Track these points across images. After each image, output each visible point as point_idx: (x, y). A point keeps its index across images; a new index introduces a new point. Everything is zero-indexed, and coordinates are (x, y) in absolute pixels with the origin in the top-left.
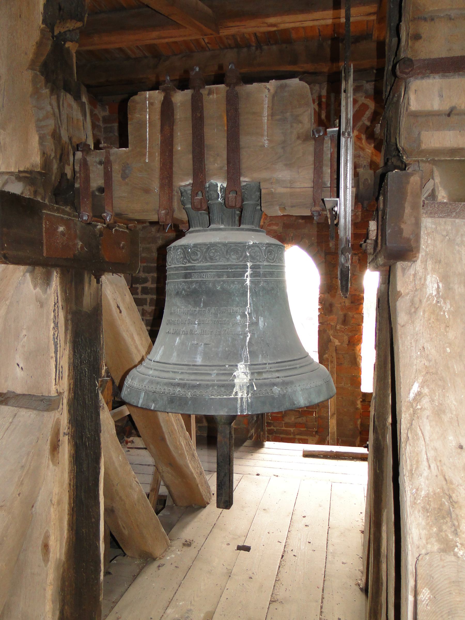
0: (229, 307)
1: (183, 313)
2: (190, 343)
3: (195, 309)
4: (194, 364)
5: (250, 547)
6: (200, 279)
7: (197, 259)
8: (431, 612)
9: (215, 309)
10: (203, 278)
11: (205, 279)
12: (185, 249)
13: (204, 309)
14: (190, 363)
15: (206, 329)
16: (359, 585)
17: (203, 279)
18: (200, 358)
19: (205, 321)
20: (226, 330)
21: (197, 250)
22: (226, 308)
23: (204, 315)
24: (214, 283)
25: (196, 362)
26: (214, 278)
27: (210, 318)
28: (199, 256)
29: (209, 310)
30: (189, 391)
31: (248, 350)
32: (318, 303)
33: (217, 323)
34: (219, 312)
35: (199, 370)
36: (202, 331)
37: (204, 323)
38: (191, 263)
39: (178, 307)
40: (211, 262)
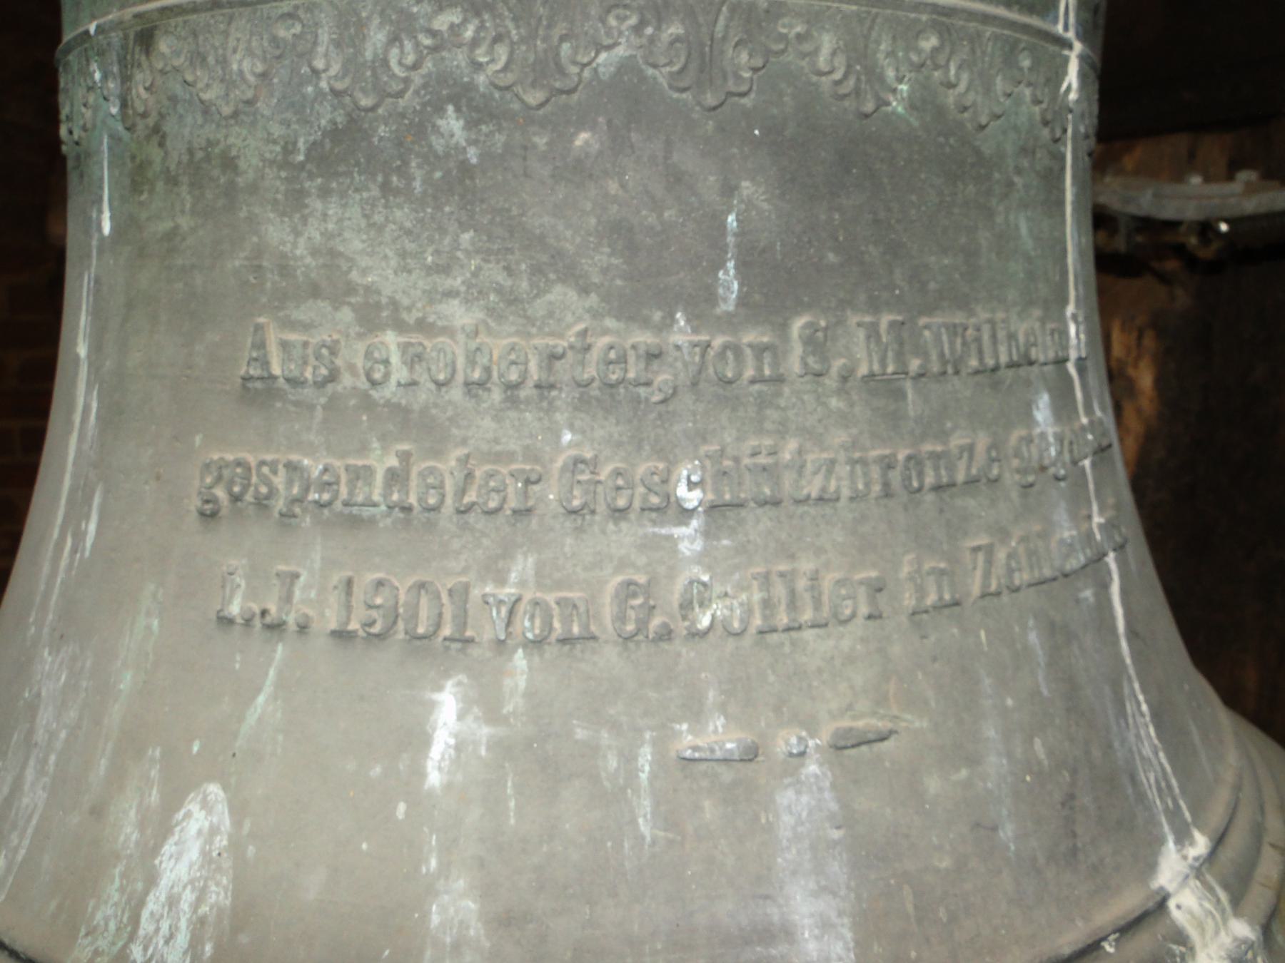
0: (983, 315)
2: (645, 756)
3: (644, 338)
8: (171, 856)
13: (750, 337)
19: (788, 480)
22: (959, 318)
23: (763, 403)
27: (840, 437)
29: (815, 343)
34: (915, 364)
36: (780, 591)
37: (776, 503)
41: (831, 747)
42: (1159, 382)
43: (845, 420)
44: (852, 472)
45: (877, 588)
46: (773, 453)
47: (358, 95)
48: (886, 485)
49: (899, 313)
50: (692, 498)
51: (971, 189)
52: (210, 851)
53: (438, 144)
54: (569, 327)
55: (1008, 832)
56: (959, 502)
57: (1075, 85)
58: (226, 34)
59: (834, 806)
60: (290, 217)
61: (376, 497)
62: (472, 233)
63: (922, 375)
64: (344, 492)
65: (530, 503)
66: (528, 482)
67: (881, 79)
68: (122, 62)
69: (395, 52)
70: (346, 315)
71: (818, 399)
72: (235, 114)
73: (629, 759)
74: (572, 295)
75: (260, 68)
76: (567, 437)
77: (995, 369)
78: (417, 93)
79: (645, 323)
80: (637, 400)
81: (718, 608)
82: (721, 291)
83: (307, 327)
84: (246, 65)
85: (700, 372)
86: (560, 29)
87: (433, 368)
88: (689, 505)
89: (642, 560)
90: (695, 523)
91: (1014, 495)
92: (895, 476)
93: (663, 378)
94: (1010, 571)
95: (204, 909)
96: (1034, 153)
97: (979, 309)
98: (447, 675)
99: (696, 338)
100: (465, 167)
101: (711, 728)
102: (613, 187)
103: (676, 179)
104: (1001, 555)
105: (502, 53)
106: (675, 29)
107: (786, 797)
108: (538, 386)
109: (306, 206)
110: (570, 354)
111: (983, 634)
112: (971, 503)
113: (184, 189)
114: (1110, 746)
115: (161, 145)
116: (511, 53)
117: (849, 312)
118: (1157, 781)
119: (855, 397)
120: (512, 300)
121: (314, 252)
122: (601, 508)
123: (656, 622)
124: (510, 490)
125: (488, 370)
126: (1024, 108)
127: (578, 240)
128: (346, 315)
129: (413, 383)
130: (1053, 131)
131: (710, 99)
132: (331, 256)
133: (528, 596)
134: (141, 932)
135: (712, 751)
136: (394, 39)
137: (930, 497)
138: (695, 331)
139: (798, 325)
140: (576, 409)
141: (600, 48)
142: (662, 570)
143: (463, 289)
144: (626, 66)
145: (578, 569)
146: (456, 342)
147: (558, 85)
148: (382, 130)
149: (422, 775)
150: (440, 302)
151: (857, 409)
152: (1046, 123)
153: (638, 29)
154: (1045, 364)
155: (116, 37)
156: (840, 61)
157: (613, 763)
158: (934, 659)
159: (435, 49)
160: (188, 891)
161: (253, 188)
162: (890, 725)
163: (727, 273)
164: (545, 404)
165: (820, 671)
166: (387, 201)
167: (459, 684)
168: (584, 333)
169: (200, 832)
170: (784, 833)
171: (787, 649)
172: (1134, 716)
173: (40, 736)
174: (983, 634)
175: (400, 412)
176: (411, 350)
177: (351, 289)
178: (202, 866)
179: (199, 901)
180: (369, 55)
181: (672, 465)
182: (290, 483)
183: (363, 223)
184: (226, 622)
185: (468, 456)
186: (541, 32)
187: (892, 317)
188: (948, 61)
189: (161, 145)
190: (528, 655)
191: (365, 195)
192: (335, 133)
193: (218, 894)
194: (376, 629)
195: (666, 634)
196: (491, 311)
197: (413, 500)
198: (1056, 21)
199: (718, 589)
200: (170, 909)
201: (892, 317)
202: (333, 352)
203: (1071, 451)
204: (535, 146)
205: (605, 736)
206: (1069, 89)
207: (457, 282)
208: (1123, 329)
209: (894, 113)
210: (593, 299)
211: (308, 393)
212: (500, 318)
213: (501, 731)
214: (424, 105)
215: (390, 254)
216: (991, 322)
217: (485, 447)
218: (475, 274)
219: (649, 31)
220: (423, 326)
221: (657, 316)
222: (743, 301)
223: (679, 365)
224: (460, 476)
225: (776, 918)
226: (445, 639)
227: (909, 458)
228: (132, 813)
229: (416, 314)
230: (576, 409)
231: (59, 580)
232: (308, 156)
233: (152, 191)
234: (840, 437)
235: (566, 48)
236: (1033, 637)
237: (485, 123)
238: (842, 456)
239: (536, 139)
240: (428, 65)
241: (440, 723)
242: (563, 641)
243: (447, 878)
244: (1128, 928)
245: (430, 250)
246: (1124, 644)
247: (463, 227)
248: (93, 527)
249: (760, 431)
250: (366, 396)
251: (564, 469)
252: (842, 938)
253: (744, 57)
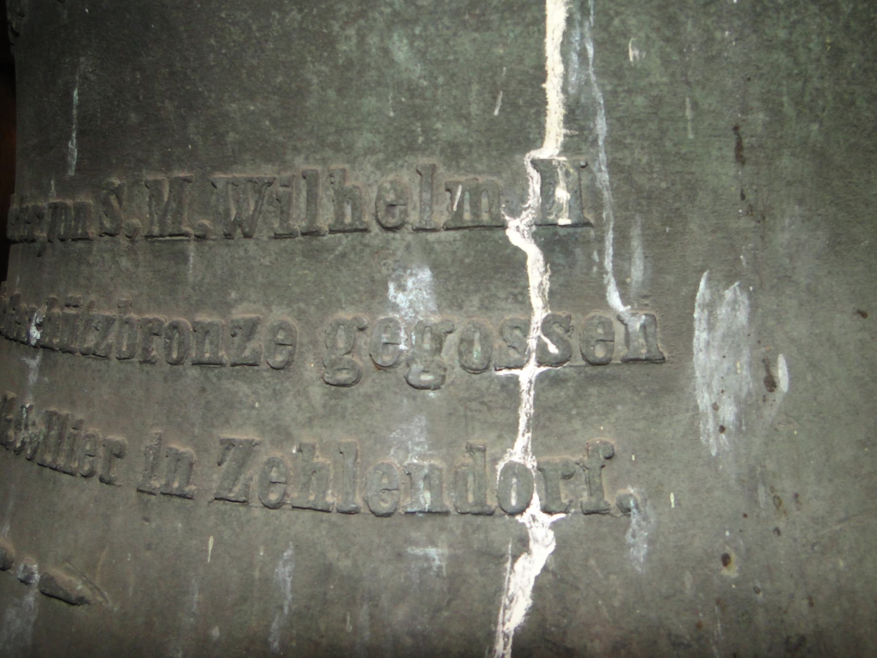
0: (300, 163)
20: (250, 448)
22: (267, 171)
41: (854, 314)
56: (227, 384)
77: (312, 233)
111: (211, 541)
112: (243, 389)
117: (144, 172)
151: (141, 269)
162: (87, 593)
163: (72, 144)
174: (211, 541)
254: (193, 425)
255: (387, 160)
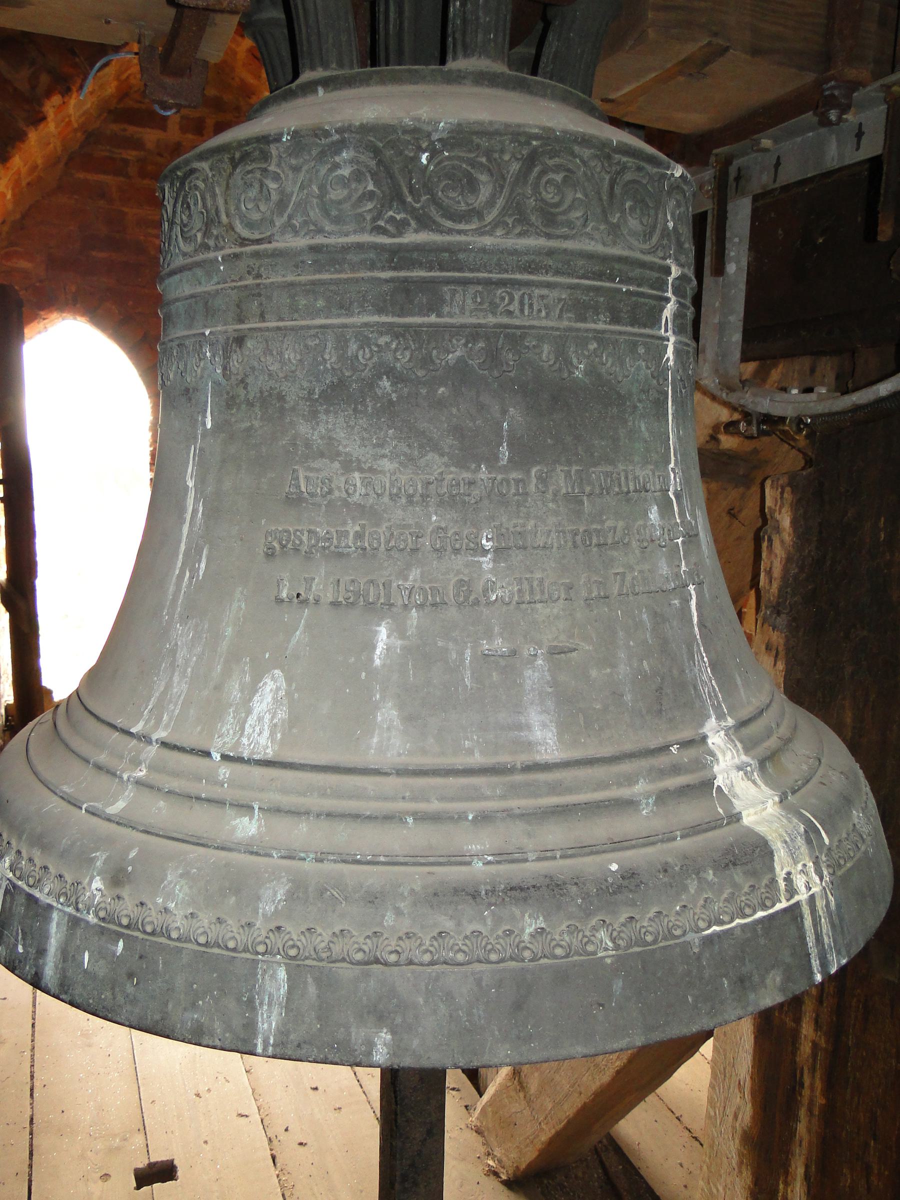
0: (621, 467)
1: (394, 497)
2: (468, 653)
3: (467, 475)
4: (523, 758)
5: (172, 1161)
6: (491, 320)
7: (478, 214)
9: (568, 474)
10: (510, 313)
11: (517, 322)
12: (389, 153)
13: (514, 475)
14: (504, 758)
15: (538, 575)
16: (496, 1174)
17: (505, 320)
18: (544, 726)
20: (623, 575)
21: (473, 163)
22: (609, 468)
23: (519, 505)
24: (561, 342)
25: (529, 746)
26: (560, 317)
27: (552, 520)
28: (485, 192)
29: (543, 480)
30: (593, 922)
31: (706, 659)
32: (148, 467)
33: (583, 541)
34: (588, 489)
35: (570, 790)
36: (526, 586)
37: (525, 548)
38: (440, 230)
39: (348, 465)
40: (549, 236)
42: (794, 522)
43: (556, 513)
44: (558, 536)
45: (569, 588)
46: (524, 526)
47: (345, 371)
48: (574, 542)
49: (580, 466)
50: (488, 545)
51: (615, 410)
52: (277, 697)
53: (379, 392)
54: (435, 470)
55: (628, 697)
56: (609, 552)
57: (671, 358)
58: (282, 342)
59: (549, 678)
60: (311, 422)
61: (350, 544)
62: (393, 430)
63: (591, 494)
64: (335, 541)
65: (419, 546)
66: (417, 537)
67: (571, 363)
68: (225, 350)
69: (361, 353)
70: (336, 465)
71: (543, 504)
72: (286, 377)
73: (461, 654)
74: (437, 457)
75: (298, 357)
76: (434, 518)
78: (370, 370)
79: (468, 469)
80: (464, 502)
81: (500, 593)
82: (501, 456)
83: (318, 470)
84: (292, 356)
85: (491, 491)
86: (433, 345)
87: (376, 488)
88: (487, 548)
89: (466, 571)
90: (489, 556)
91: (637, 551)
92: (578, 538)
93: (476, 492)
94: (633, 586)
95: (275, 721)
96: (648, 391)
97: (620, 465)
98: (382, 619)
99: (490, 476)
100: (390, 402)
101: (496, 643)
102: (454, 411)
103: (481, 407)
104: (629, 578)
105: (408, 354)
106: (481, 344)
107: (528, 673)
108: (422, 496)
109: (319, 418)
110: (435, 482)
112: (615, 554)
113: (257, 410)
114: (683, 671)
115: (245, 388)
116: (412, 355)
118: (709, 692)
119: (560, 503)
120: (411, 459)
121: (322, 438)
122: (449, 548)
123: (472, 598)
124: (410, 540)
125: (400, 489)
126: (642, 372)
127: (439, 433)
128: (336, 465)
129: (367, 495)
130: (658, 381)
131: (496, 373)
132: (330, 440)
133: (417, 585)
134: (246, 733)
135: (497, 651)
136: (361, 347)
137: (595, 549)
138: (490, 473)
139: (534, 471)
140: (438, 506)
141: (449, 352)
142: (475, 575)
143: (389, 454)
144: (460, 360)
145: (439, 575)
146: (386, 477)
147: (431, 368)
148: (354, 386)
149: (372, 661)
150: (379, 460)
151: (561, 508)
152: (653, 377)
153: (465, 345)
154: (655, 492)
155: (222, 339)
156: (552, 356)
157: (454, 656)
158: (596, 621)
159: (379, 352)
160: (267, 714)
161: (293, 409)
164: (425, 504)
165: (544, 621)
166: (356, 416)
167: (388, 623)
168: (441, 473)
169: (271, 690)
170: (528, 687)
171: (529, 611)
172: (699, 661)
173: (180, 661)
175: (361, 507)
176: (366, 480)
177: (339, 454)
178: (274, 704)
179: (273, 718)
180: (349, 354)
181: (480, 530)
182: (309, 539)
183: (345, 425)
184: (280, 601)
185: (391, 526)
186: (424, 346)
187: (578, 468)
188: (602, 354)
189: (245, 388)
190: (417, 611)
191: (346, 413)
192: (333, 386)
193: (282, 714)
194: (351, 600)
195: (477, 602)
196: (401, 463)
197: (366, 545)
198: (660, 328)
199: (499, 585)
200: (259, 722)
201: (578, 468)
202: (330, 481)
203: (669, 535)
204: (421, 393)
205: (451, 645)
206: (668, 359)
207: (387, 451)
208: (772, 487)
209: (577, 377)
210: (446, 459)
211: (318, 499)
212: (405, 467)
213: (406, 643)
214: (373, 376)
215: (357, 439)
216: (626, 471)
217: (398, 522)
218: (394, 448)
219: (470, 345)
220: (371, 470)
221: (473, 466)
222: (510, 460)
223: (483, 487)
224: (388, 535)
225: (523, 721)
226: (382, 604)
227: (585, 531)
228: (237, 686)
229: (368, 465)
230: (438, 506)
231: (183, 592)
232: (320, 396)
233: (238, 409)
234: (552, 520)
235: (435, 352)
236: (645, 616)
237: (400, 384)
238: (554, 529)
239: (422, 391)
240: (375, 359)
241: (380, 639)
242: (433, 605)
243: (384, 702)
244: (686, 744)
245: (375, 437)
246: (696, 629)
247: (389, 427)
248: (203, 565)
249: (518, 517)
250: (345, 500)
251: (432, 532)
252: (552, 731)
253: (511, 355)
254: (600, 570)
255: (642, 467)
